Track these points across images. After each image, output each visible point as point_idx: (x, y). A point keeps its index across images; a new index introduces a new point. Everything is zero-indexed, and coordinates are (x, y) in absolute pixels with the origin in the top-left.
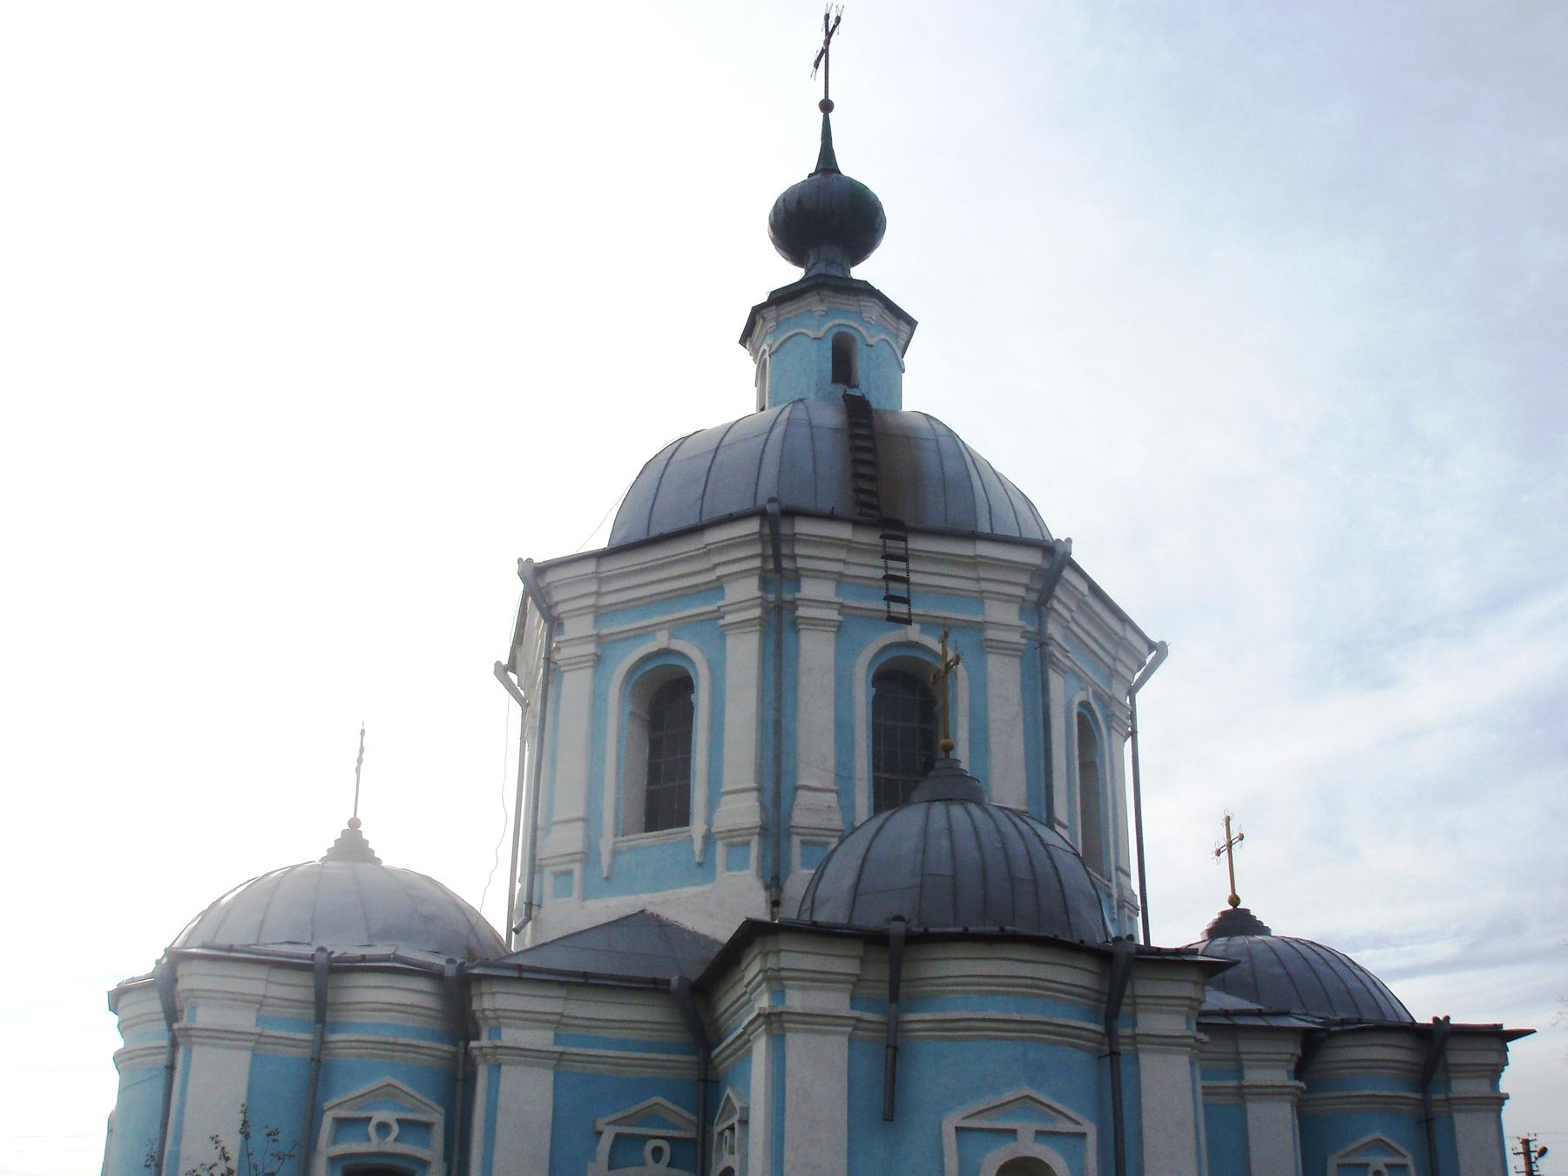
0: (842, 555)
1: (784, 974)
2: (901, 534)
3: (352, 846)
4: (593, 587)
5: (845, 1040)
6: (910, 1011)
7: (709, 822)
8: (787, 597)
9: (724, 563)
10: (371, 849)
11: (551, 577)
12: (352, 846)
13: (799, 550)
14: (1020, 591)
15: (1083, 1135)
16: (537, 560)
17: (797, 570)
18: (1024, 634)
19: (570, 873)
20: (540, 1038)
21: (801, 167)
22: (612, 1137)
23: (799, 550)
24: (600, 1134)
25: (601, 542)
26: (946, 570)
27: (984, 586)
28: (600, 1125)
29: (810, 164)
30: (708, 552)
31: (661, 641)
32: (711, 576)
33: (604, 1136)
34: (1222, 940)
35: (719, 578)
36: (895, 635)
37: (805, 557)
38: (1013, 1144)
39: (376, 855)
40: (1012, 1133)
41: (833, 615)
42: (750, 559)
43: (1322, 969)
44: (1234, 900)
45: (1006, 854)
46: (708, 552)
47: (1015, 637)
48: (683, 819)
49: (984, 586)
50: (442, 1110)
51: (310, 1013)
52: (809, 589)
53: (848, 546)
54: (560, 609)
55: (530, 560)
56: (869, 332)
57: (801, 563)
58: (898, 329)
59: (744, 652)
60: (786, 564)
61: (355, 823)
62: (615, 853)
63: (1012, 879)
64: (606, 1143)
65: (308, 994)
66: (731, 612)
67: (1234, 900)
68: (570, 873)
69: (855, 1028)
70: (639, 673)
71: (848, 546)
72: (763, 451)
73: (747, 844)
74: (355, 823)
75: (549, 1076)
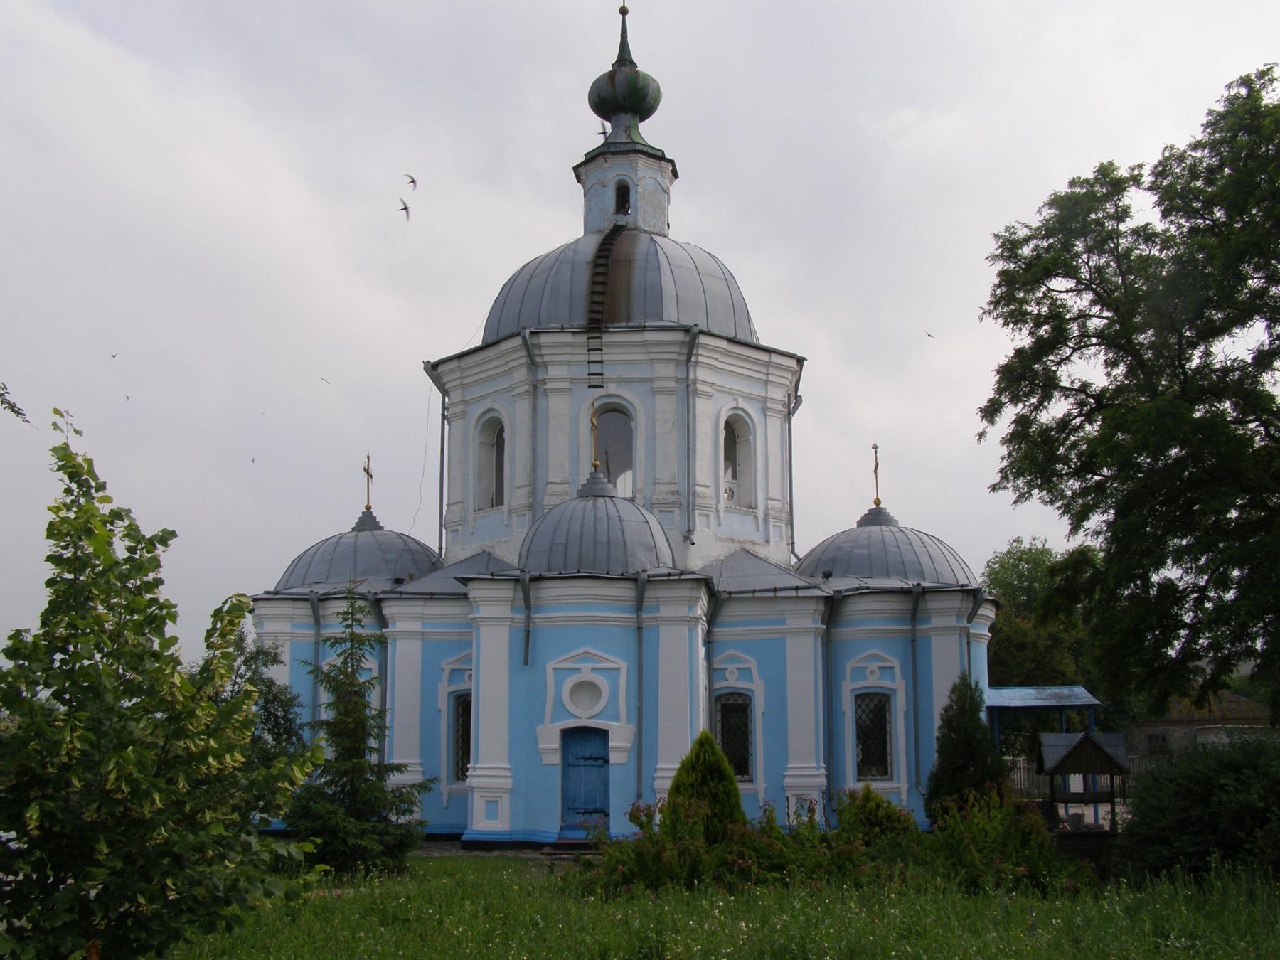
0: (569, 350)
1: (477, 599)
2: (598, 335)
3: (368, 522)
4: (458, 375)
5: (507, 629)
6: (537, 613)
7: (510, 503)
8: (540, 377)
9: (512, 360)
10: (10, 659)
11: (441, 369)
12: (368, 522)
13: (544, 351)
14: (674, 356)
15: (619, 669)
16: (432, 361)
17: (545, 362)
18: (678, 380)
19: (457, 530)
20: (416, 626)
21: (605, 62)
22: (449, 671)
23: (544, 351)
24: (443, 670)
25: (478, 342)
26: (620, 350)
27: (652, 356)
28: (443, 664)
29: (614, 56)
30: (503, 355)
31: (488, 404)
32: (506, 368)
33: (445, 671)
34: (867, 529)
35: (510, 369)
36: (599, 392)
37: (547, 354)
38: (579, 675)
39: (381, 524)
40: (578, 670)
41: (566, 385)
42: (521, 357)
43: (916, 543)
44: (877, 502)
45: (595, 529)
46: (503, 355)
47: (672, 384)
48: (502, 504)
49: (652, 356)
50: (377, 662)
51: (312, 620)
52: (553, 371)
53: (572, 345)
54: (447, 386)
55: (428, 362)
56: (643, 174)
57: (546, 358)
58: (661, 167)
59: (523, 407)
60: (538, 359)
61: (368, 508)
62: (475, 519)
63: (595, 543)
64: (446, 675)
65: (310, 612)
66: (517, 387)
67: (877, 502)
68: (457, 530)
69: (512, 622)
70: (480, 424)
71: (572, 345)
72: (546, 282)
73: (524, 515)
74: (368, 508)
75: (419, 643)
